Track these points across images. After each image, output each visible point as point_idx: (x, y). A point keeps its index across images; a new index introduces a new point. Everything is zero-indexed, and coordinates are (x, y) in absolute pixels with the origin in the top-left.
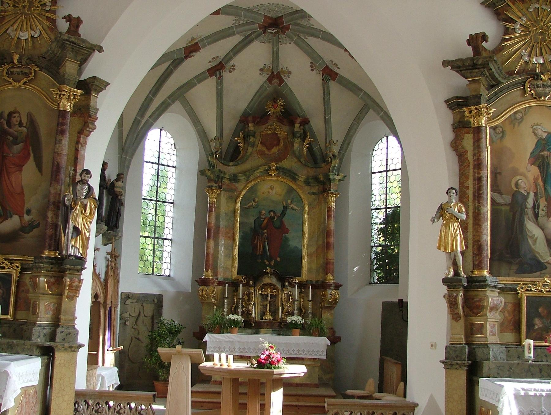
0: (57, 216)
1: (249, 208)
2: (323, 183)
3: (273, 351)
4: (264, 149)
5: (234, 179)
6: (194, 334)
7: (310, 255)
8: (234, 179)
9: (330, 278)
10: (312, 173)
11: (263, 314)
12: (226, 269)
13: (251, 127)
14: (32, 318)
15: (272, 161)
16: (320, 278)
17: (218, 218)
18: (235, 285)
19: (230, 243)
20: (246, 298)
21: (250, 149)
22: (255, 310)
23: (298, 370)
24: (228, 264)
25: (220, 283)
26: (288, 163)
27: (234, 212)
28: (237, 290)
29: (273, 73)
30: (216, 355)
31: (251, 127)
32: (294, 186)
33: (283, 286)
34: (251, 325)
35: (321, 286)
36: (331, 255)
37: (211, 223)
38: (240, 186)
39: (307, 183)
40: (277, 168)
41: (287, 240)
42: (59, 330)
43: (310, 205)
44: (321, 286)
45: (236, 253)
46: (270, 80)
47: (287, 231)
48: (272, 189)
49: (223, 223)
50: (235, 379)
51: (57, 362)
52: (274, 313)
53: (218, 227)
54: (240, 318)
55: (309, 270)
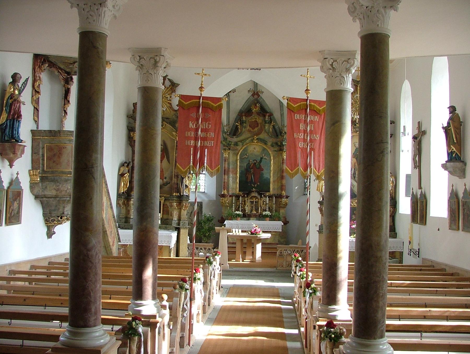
0: (178, 180)
1: (244, 159)
2: (280, 146)
3: (257, 228)
4: (251, 129)
5: (236, 144)
6: (219, 221)
7: (274, 181)
8: (236, 144)
9: (284, 193)
10: (275, 140)
11: (252, 211)
12: (233, 189)
13: (244, 118)
14: (170, 217)
15: (255, 135)
16: (279, 193)
17: (229, 164)
18: (238, 197)
19: (235, 176)
20: (243, 203)
21: (244, 129)
22: (247, 209)
23: (268, 236)
24: (234, 185)
25: (230, 196)
26: (262, 136)
27: (237, 160)
28: (239, 199)
29: (254, 92)
30: (234, 230)
31: (244, 118)
32: (266, 148)
33: (261, 197)
34: (246, 216)
35: (279, 197)
36: (284, 182)
37: (233, 178)
38: (239, 148)
39: (272, 146)
40: (257, 139)
41: (263, 174)
42: (181, 221)
43: (273, 156)
44: (279, 197)
45: (238, 181)
46: (253, 95)
47: (262, 170)
48: (255, 149)
49: (231, 167)
50: (241, 239)
51: (181, 233)
52: (257, 210)
53: (229, 168)
54: (241, 213)
55: (274, 189)
